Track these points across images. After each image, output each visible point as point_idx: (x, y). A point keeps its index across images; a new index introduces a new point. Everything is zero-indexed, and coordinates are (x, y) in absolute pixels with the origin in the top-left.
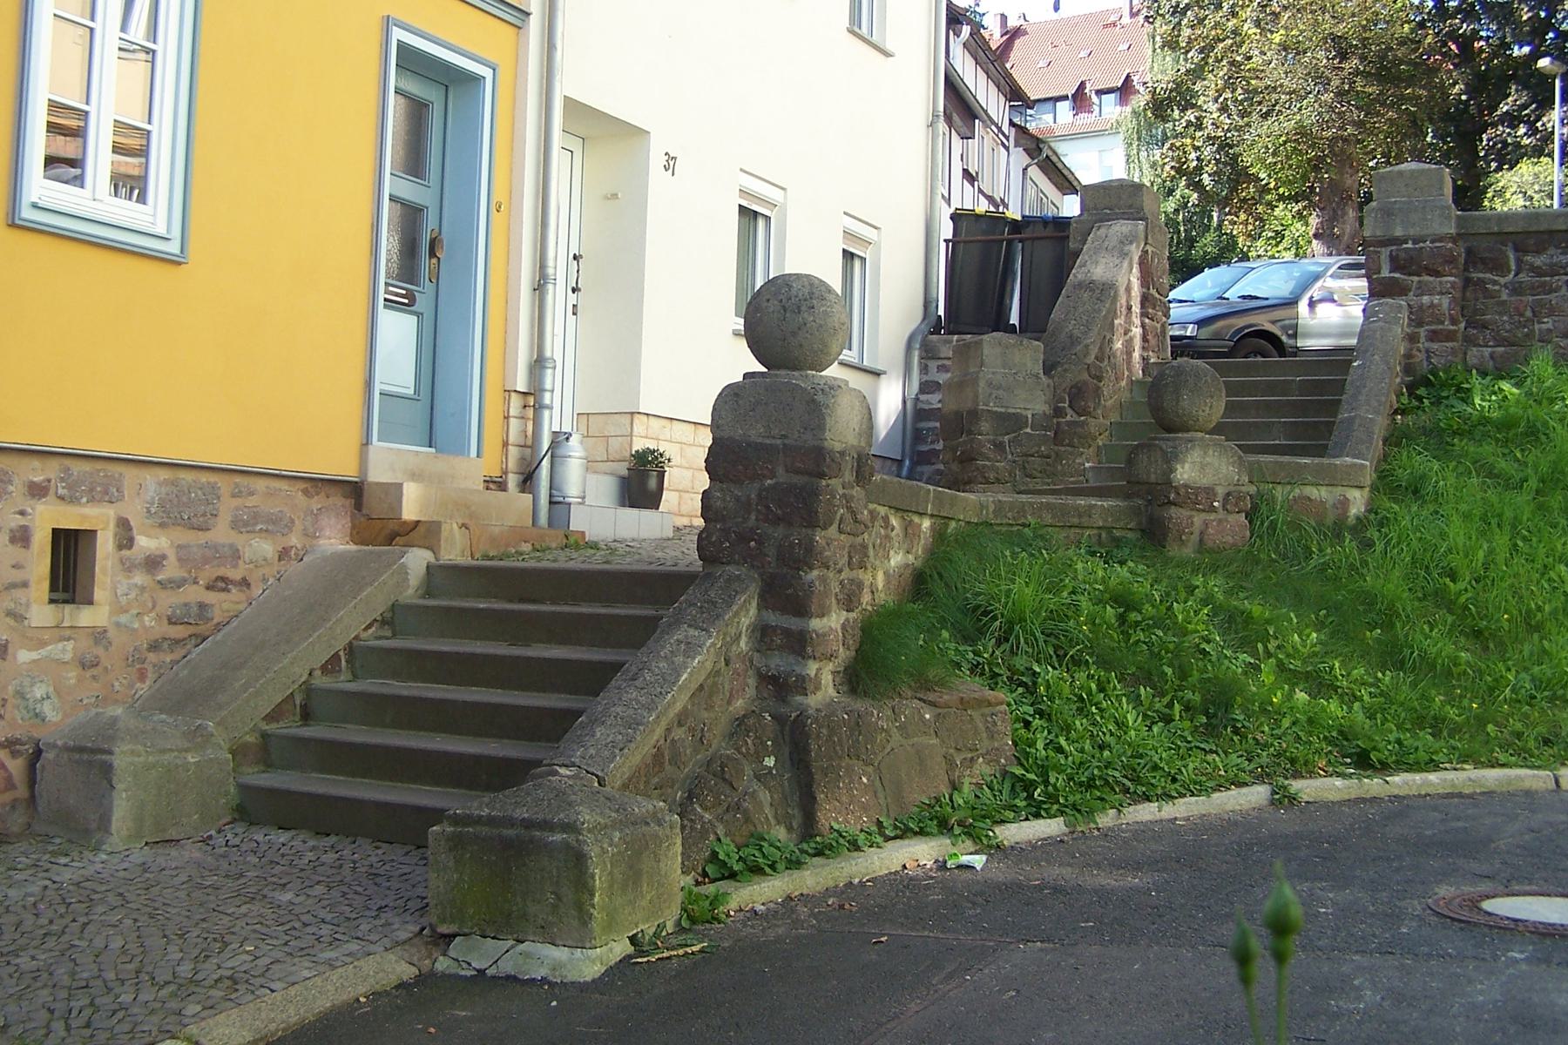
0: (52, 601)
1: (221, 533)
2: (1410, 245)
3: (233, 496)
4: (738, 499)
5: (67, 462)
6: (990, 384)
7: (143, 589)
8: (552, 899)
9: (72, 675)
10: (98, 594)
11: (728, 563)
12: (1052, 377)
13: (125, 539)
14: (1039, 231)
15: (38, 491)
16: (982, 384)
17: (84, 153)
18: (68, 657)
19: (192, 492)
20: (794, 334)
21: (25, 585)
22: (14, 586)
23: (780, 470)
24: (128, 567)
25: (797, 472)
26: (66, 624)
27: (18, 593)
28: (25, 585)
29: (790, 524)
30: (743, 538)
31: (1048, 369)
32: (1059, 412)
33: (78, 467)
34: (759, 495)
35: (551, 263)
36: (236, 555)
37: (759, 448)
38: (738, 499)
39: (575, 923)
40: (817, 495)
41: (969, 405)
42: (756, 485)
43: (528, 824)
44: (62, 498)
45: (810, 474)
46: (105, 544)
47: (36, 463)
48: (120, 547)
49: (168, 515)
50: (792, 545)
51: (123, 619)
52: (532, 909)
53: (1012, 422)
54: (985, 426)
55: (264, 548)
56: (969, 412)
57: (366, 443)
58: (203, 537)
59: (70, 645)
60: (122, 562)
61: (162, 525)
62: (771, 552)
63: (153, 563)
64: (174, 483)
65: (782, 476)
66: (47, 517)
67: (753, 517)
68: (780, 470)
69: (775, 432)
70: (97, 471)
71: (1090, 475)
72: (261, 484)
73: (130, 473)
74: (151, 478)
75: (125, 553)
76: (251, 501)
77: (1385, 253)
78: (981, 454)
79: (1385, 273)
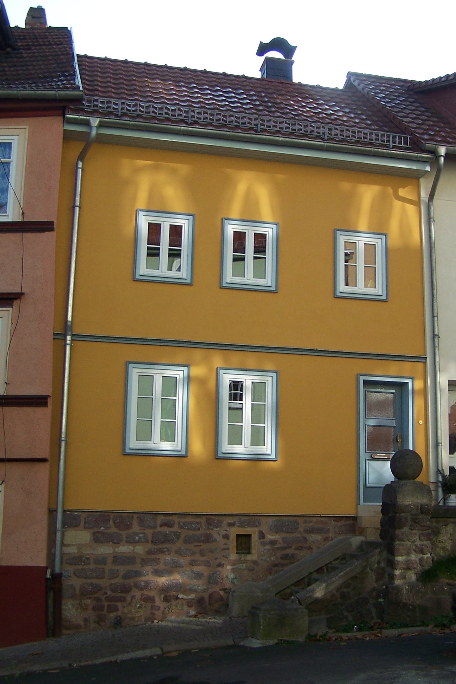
0: (237, 553)
1: (159, 529)
3: (304, 523)
5: (241, 517)
7: (269, 550)
9: (245, 573)
10: (253, 551)
13: (262, 535)
15: (231, 525)
17: (57, 506)
18: (244, 568)
19: (285, 523)
21: (228, 549)
22: (224, 549)
24: (264, 544)
26: (242, 559)
27: (227, 551)
28: (228, 549)
33: (243, 518)
35: (439, 438)
36: (306, 539)
44: (239, 526)
46: (255, 538)
47: (230, 518)
48: (260, 538)
49: (277, 529)
51: (264, 558)
55: (317, 537)
57: (358, 503)
58: (170, 529)
59: (244, 565)
60: (261, 543)
61: (276, 532)
63: (273, 543)
64: (277, 520)
66: (234, 532)
70: (252, 519)
72: (314, 519)
73: (263, 519)
74: (270, 520)
75: (262, 540)
76: (311, 524)
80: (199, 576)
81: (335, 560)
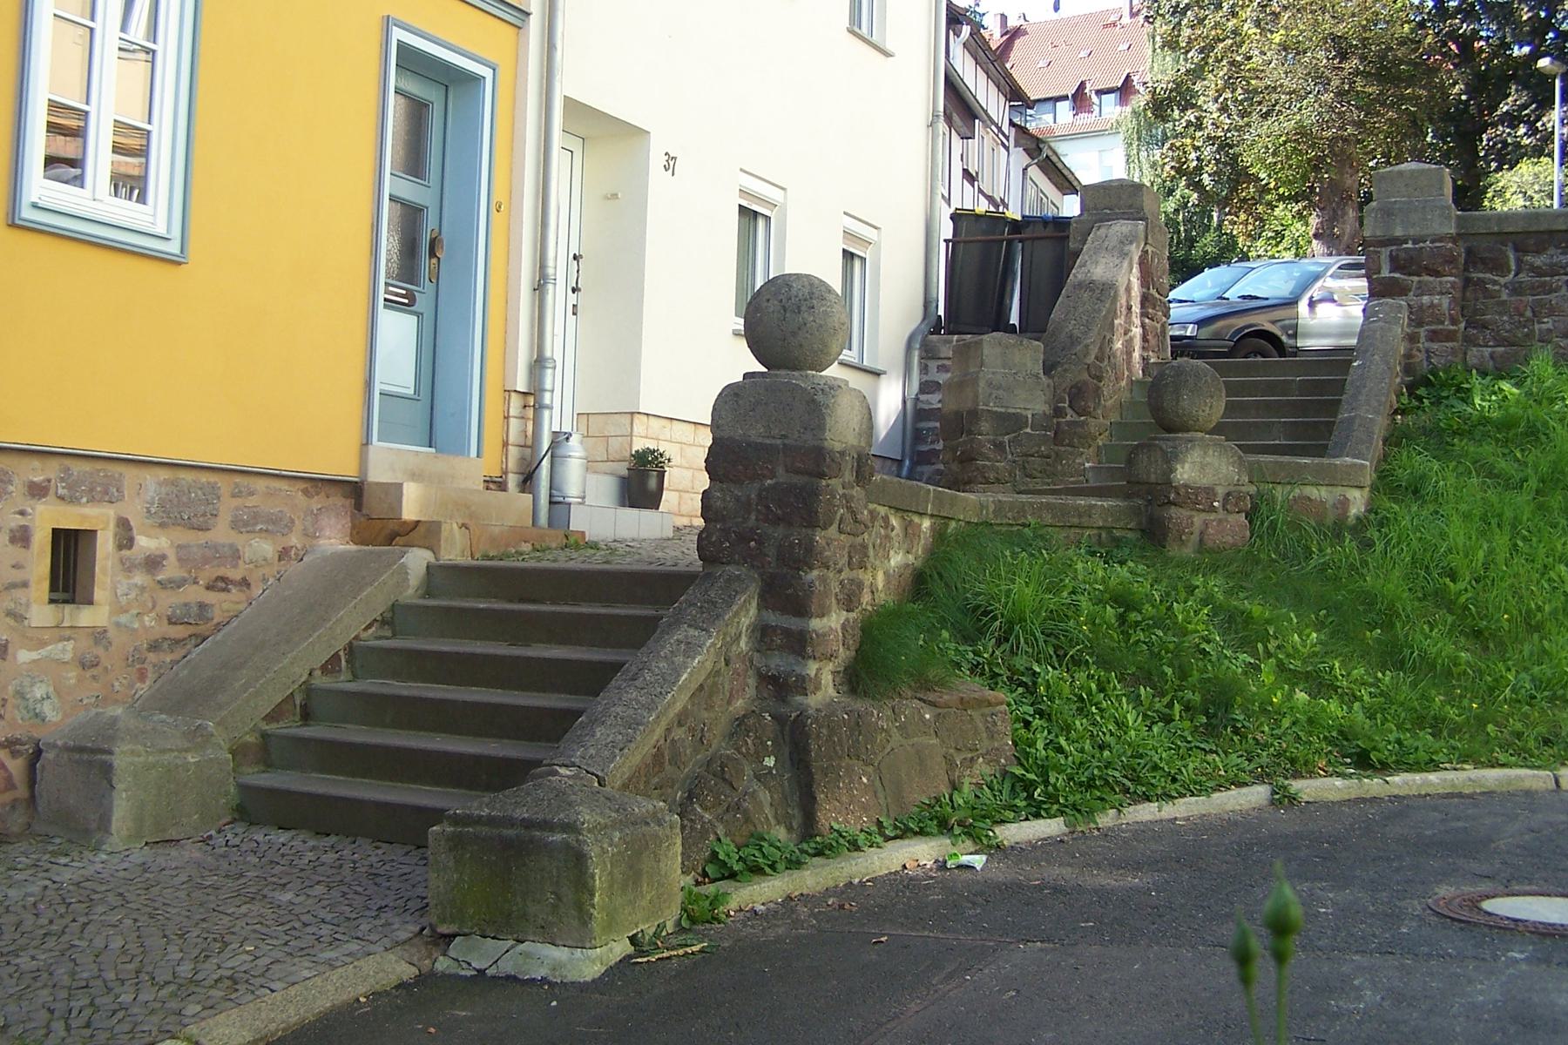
0: (52, 601)
1: (221, 533)
2: (1410, 245)
3: (233, 496)
4: (738, 499)
5: (67, 462)
6: (990, 384)
7: (143, 589)
8: (552, 899)
9: (72, 675)
10: (98, 594)
11: (728, 563)
12: (1052, 377)
13: (125, 539)
14: (1039, 231)
15: (38, 491)
16: (982, 384)
18: (68, 657)
19: (192, 492)
20: (794, 334)
21: (25, 585)
22: (14, 586)
23: (780, 470)
24: (128, 567)
25: (797, 472)
26: (66, 624)
27: (18, 593)
28: (25, 585)
29: (790, 524)
30: (743, 538)
31: (1048, 369)
32: (1059, 412)
33: (78, 467)
34: (759, 495)
35: (551, 263)
36: (236, 555)
37: (759, 448)
38: (738, 499)
39: (575, 923)
40: (817, 495)
41: (969, 405)
42: (756, 485)
43: (528, 824)
44: (62, 498)
45: (810, 474)
46: (105, 544)
47: (36, 463)
48: (120, 547)
49: (168, 515)
50: (792, 545)
51: (123, 619)
52: (532, 909)
53: (1012, 422)
54: (985, 426)
55: (264, 548)
56: (969, 412)
57: (366, 443)
58: (203, 537)
59: (70, 645)
60: (122, 562)
61: (162, 525)
62: (771, 552)
63: (153, 563)
64: (174, 483)
65: (782, 476)
66: (47, 517)
67: (753, 517)
68: (780, 470)
69: (775, 432)
70: (97, 471)
71: (1090, 475)
72: (261, 484)
73: (130, 473)
74: (151, 478)
75: (125, 553)
76: (251, 501)
77: (1385, 253)
78: (981, 454)
79: (1385, 273)
80: (1337, 1016)
81: (366, 629)
